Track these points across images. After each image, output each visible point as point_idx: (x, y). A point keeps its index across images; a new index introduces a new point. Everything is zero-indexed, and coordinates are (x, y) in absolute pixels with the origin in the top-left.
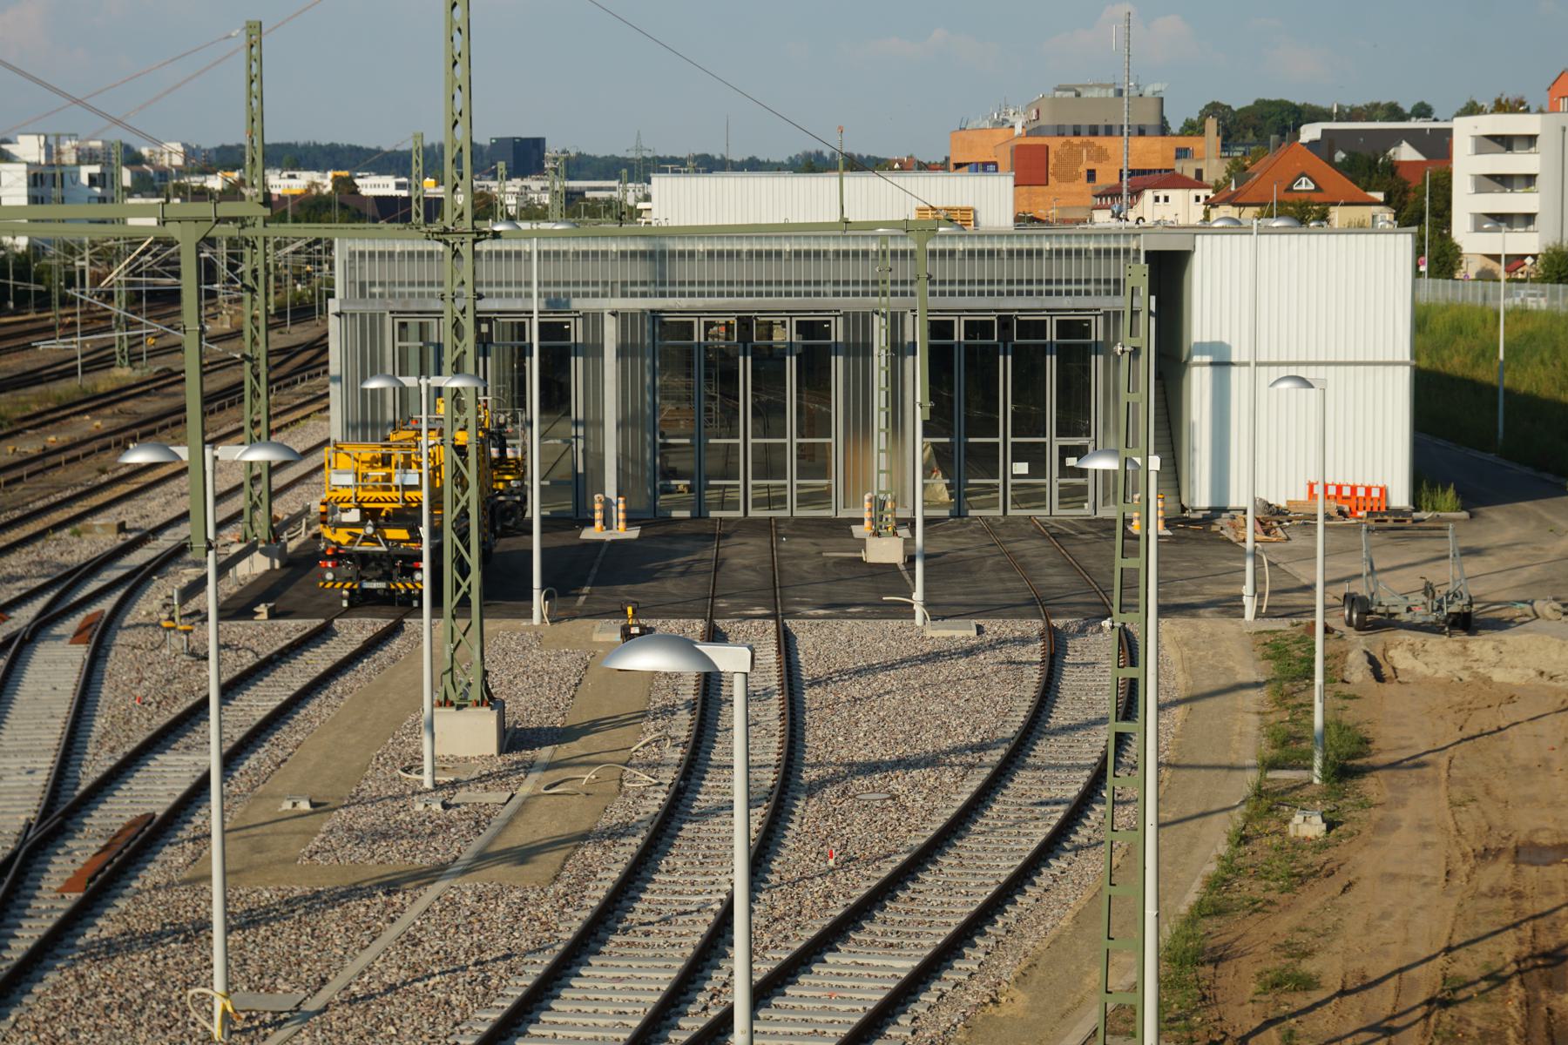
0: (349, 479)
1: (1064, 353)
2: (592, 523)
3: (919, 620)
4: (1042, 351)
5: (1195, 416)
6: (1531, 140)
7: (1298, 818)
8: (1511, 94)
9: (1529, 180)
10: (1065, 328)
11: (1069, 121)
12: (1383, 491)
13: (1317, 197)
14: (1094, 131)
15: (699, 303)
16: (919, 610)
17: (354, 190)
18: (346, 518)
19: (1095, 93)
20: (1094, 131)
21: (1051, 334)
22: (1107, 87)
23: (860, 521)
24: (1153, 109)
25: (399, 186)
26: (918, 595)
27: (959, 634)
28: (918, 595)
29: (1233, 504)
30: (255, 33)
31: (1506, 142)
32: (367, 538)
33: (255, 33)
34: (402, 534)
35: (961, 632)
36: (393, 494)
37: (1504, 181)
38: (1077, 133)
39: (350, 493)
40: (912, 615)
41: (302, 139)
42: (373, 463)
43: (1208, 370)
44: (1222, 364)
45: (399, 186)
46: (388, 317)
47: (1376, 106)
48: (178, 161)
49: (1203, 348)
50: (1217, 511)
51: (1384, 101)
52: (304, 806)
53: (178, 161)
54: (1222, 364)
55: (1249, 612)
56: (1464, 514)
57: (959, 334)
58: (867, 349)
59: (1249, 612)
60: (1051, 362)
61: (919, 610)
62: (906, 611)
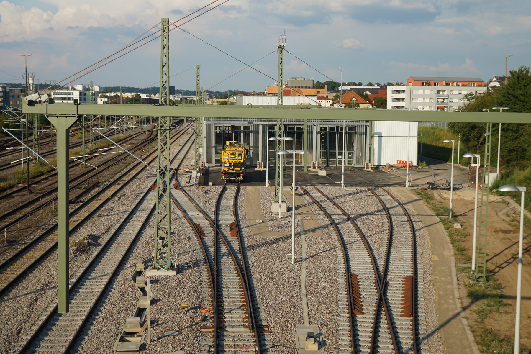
0: (227, 157)
1: (245, 133)
2: (257, 167)
3: (267, 186)
4: (240, 132)
5: (375, 147)
6: (404, 91)
7: (455, 225)
8: (399, 82)
9: (403, 99)
10: (298, 128)
11: (294, 85)
12: (412, 162)
13: (357, 102)
14: (299, 87)
15: (242, 123)
16: (343, 185)
17: (140, 97)
18: (226, 165)
19: (300, 79)
20: (299, 87)
21: (295, 130)
22: (302, 78)
23: (310, 167)
24: (312, 82)
25: (147, 96)
26: (342, 182)
27: (353, 189)
28: (342, 182)
29: (382, 164)
30: (198, 67)
31: (398, 92)
32: (231, 169)
33: (198, 67)
34: (239, 169)
35: (353, 189)
36: (236, 161)
37: (398, 99)
38: (296, 87)
39: (227, 160)
40: (341, 186)
41: (112, 86)
42: (231, 154)
43: (377, 138)
44: (380, 137)
45: (147, 96)
46: (318, 126)
47: (351, 83)
48: (98, 90)
49: (377, 133)
50: (379, 166)
51: (352, 82)
52: (261, 221)
53: (98, 90)
54: (380, 137)
55: (407, 186)
56: (427, 167)
57: (328, 130)
58: (258, 132)
59: (407, 186)
60: (242, 135)
61: (343, 185)
62: (340, 185)
